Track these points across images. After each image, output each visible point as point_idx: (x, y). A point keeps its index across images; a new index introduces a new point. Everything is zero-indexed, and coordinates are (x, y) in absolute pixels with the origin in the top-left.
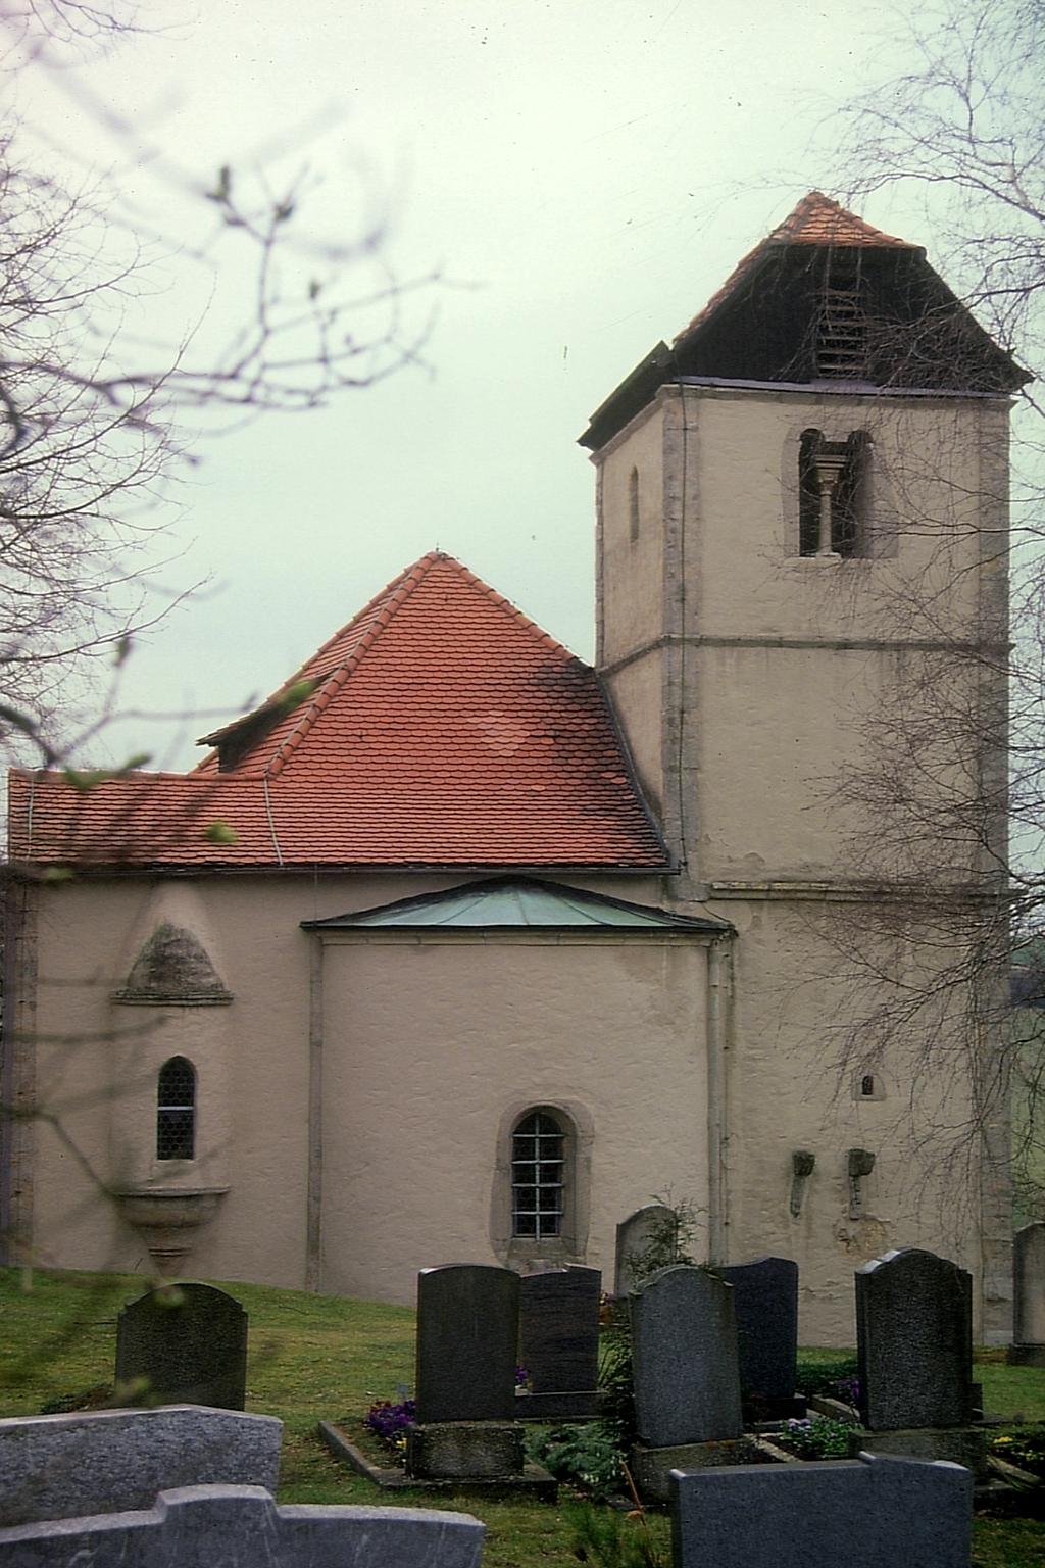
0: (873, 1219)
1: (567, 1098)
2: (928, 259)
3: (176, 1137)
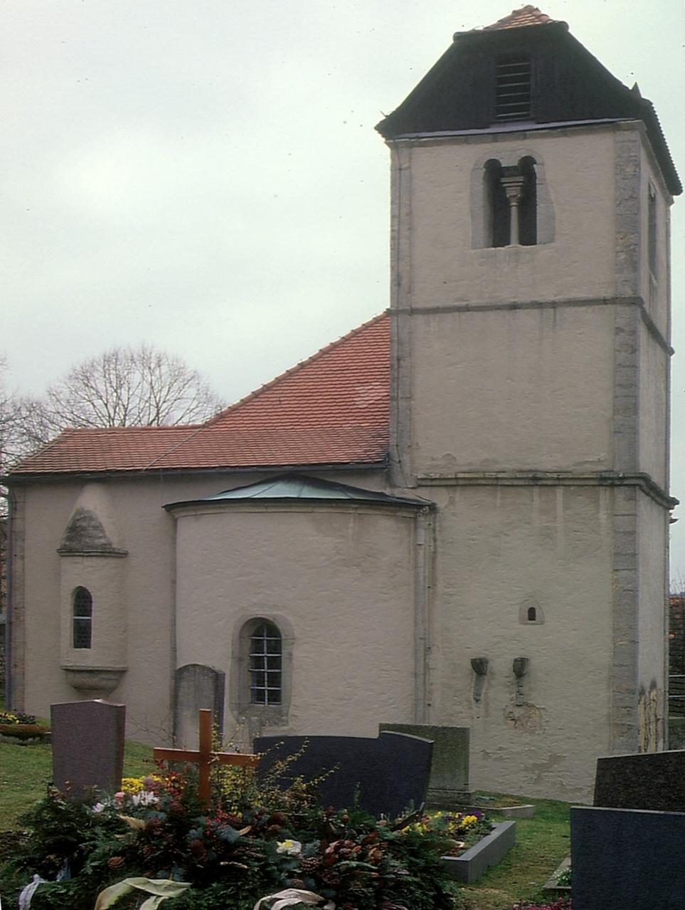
0: (533, 706)
1: (275, 613)
2: (570, 31)
3: (82, 637)
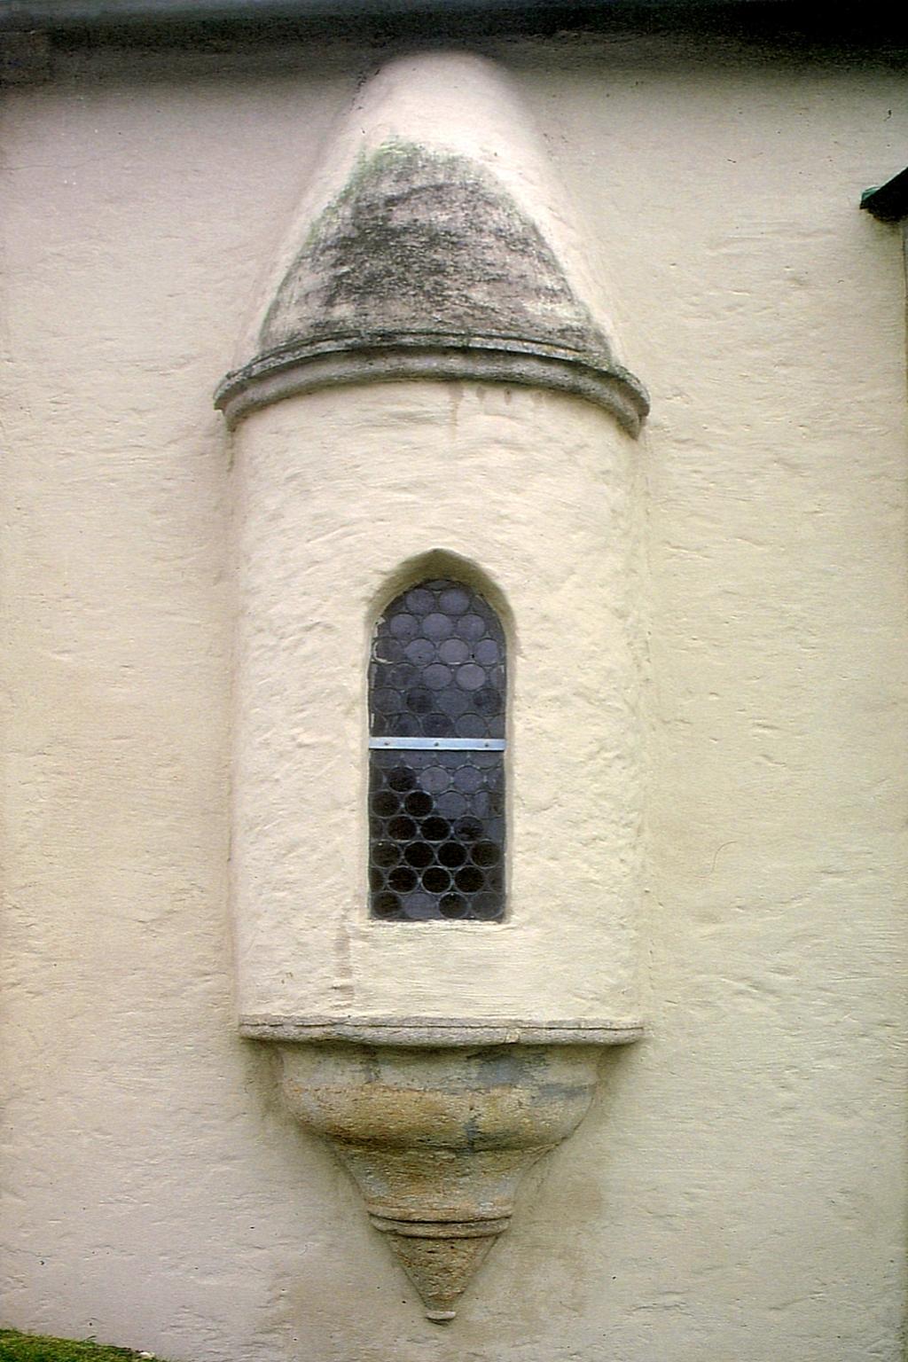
3: (436, 851)
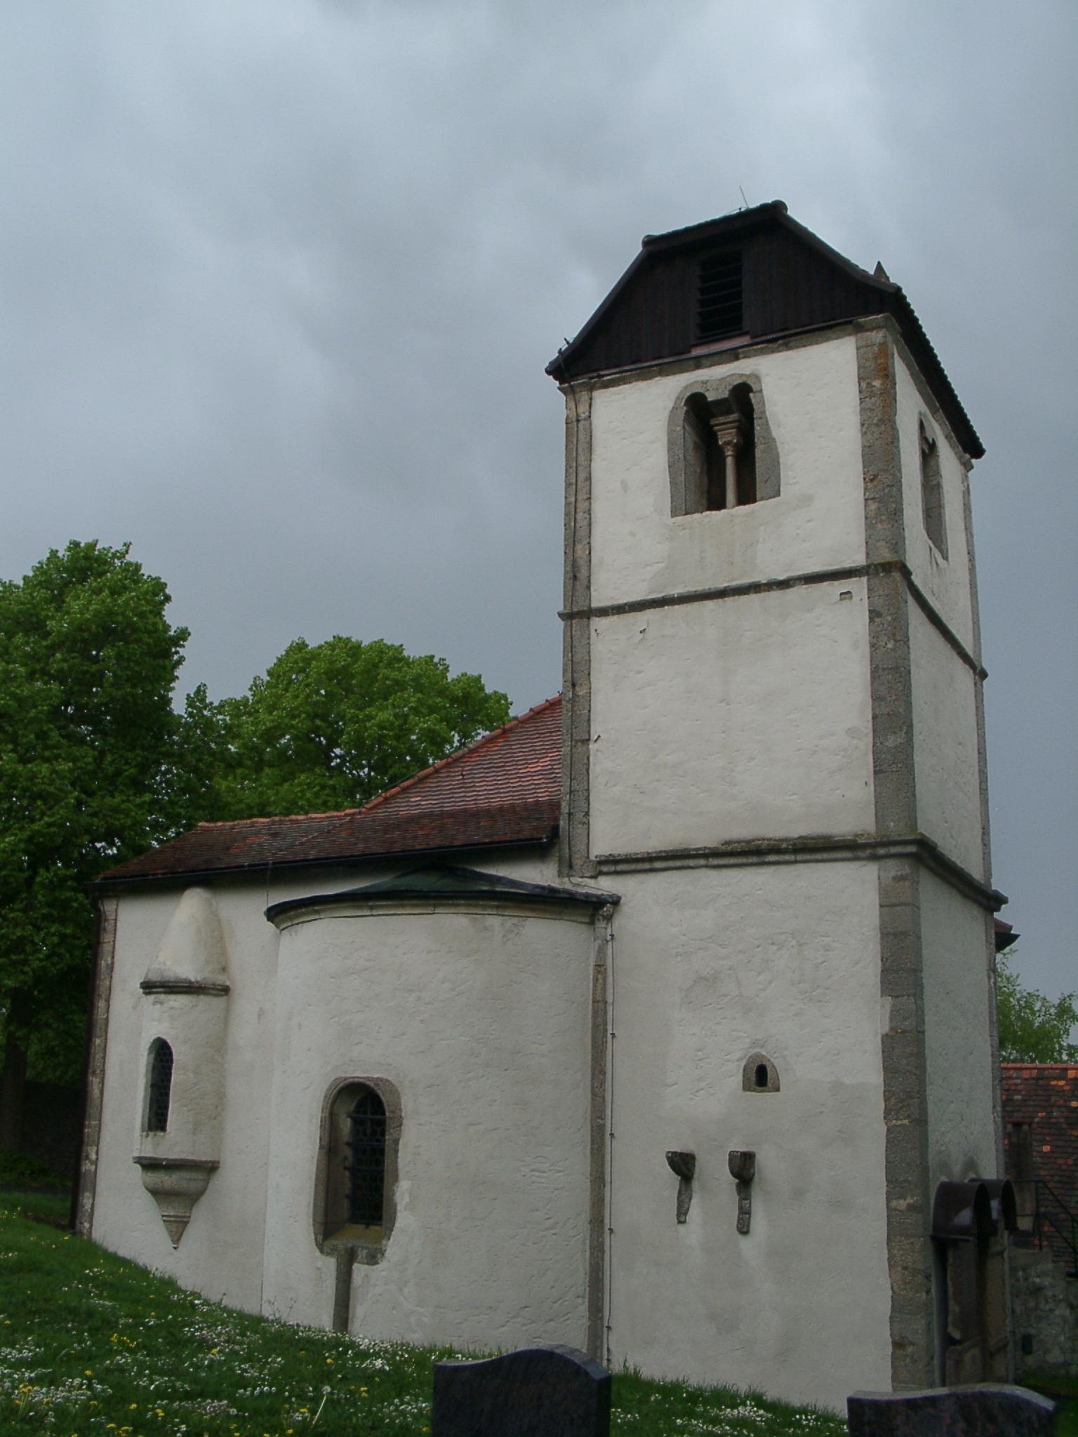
2: (789, 213)
